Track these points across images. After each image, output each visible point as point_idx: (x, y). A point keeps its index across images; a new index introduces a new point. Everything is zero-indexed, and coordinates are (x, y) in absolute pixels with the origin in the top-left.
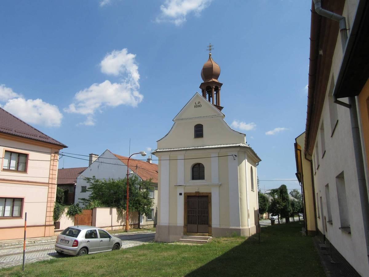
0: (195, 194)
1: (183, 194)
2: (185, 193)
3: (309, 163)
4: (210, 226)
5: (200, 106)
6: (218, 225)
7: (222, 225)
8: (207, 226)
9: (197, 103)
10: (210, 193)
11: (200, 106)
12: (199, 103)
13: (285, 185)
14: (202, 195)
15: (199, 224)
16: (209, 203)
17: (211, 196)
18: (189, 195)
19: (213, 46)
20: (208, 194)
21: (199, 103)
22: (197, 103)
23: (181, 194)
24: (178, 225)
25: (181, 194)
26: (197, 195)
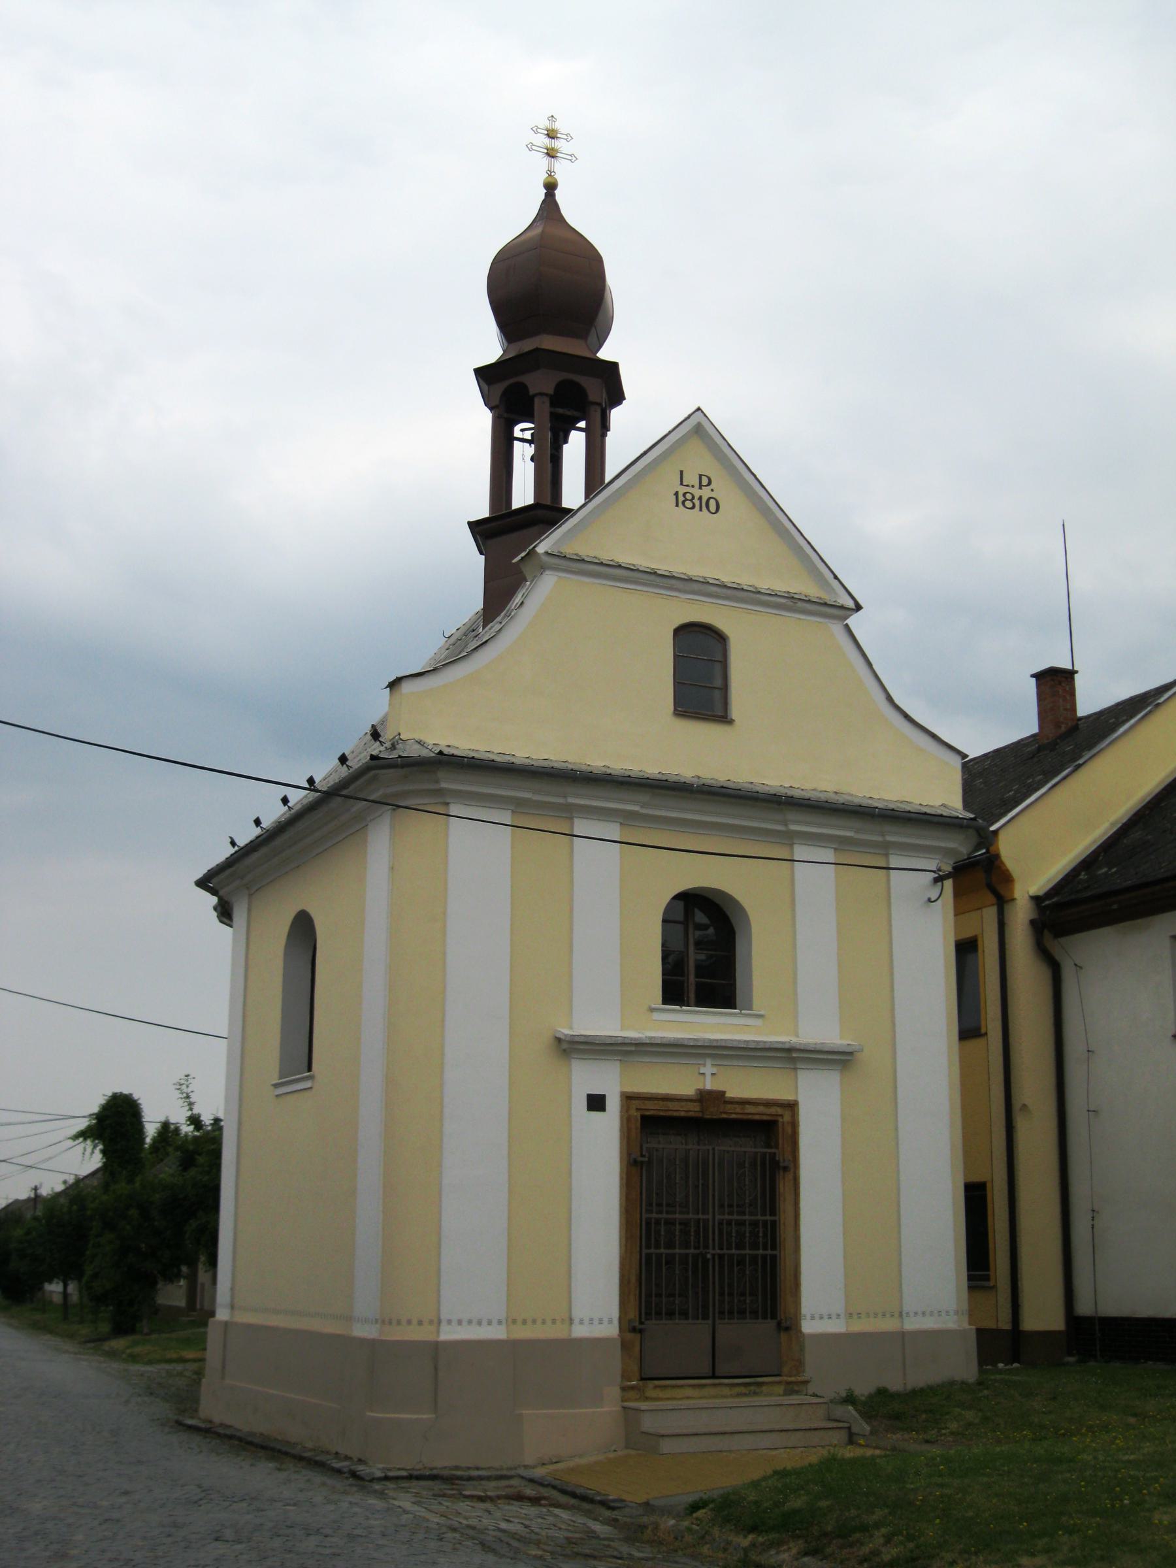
0: (694, 1109)
1: (613, 1104)
2: (628, 1099)
3: (1044, 973)
4: (788, 1325)
5: (712, 504)
6: (500, 1322)
7: (554, 1322)
8: (771, 1324)
9: (691, 478)
10: (792, 1106)
11: (711, 506)
12: (705, 481)
13: (136, 1096)
14: (734, 1113)
15: (722, 1313)
16: (786, 1169)
17: (794, 1125)
18: (652, 1108)
19: (569, 138)
20: (773, 1110)
21: (705, 481)
22: (691, 478)
23: (596, 1103)
24: (580, 1331)
25: (596, 1103)
26: (712, 1113)
